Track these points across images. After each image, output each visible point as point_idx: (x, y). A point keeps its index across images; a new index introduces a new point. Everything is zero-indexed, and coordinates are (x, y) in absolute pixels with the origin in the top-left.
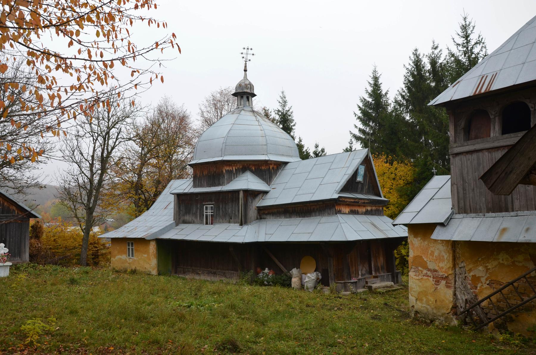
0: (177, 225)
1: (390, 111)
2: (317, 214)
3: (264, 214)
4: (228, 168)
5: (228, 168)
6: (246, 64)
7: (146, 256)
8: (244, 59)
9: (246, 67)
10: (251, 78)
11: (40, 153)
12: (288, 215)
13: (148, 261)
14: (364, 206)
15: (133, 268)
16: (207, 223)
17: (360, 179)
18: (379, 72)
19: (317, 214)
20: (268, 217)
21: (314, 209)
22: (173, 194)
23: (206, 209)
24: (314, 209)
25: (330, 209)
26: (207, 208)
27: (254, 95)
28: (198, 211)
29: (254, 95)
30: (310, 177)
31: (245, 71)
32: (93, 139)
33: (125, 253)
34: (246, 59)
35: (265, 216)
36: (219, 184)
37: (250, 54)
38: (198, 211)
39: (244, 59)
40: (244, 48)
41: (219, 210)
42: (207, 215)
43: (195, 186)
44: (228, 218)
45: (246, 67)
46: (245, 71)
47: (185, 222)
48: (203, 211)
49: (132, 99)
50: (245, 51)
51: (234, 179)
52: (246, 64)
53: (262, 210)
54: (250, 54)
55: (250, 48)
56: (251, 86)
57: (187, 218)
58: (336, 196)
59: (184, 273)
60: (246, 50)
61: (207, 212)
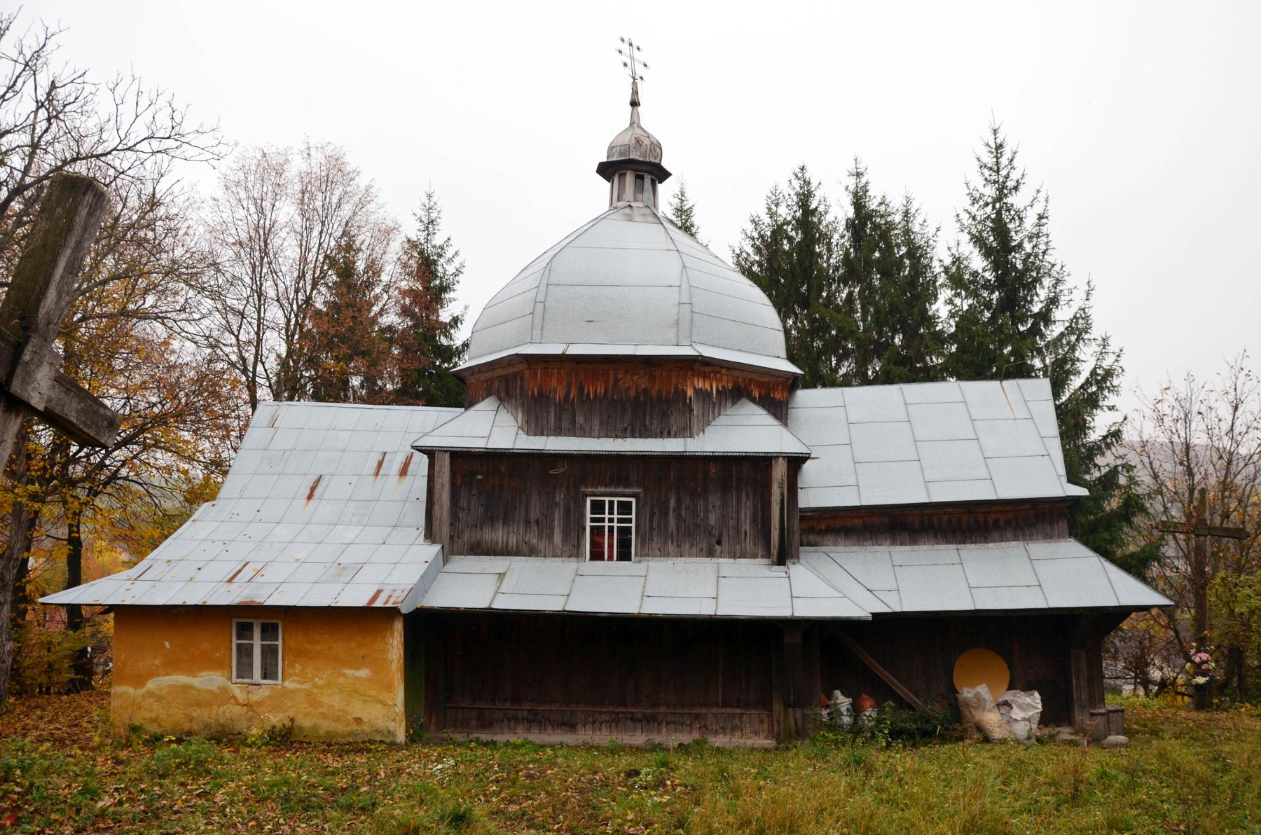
0: (446, 561)
2: (1009, 535)
3: (811, 530)
4: (700, 384)
5: (700, 384)
6: (634, 83)
7: (364, 673)
9: (635, 92)
10: (654, 123)
11: (346, 272)
12: (906, 536)
13: (370, 694)
15: (276, 719)
16: (597, 555)
18: (813, 175)
19: (1009, 535)
20: (829, 539)
21: (996, 522)
23: (598, 507)
24: (996, 522)
25: (1051, 523)
28: (558, 516)
31: (634, 104)
33: (221, 665)
35: (812, 538)
36: (665, 432)
38: (558, 516)
40: (623, 40)
41: (666, 514)
44: (712, 543)
45: (635, 92)
46: (634, 104)
47: (478, 549)
48: (583, 516)
51: (714, 418)
52: (634, 83)
53: (810, 518)
56: (657, 147)
57: (498, 535)
59: (486, 725)
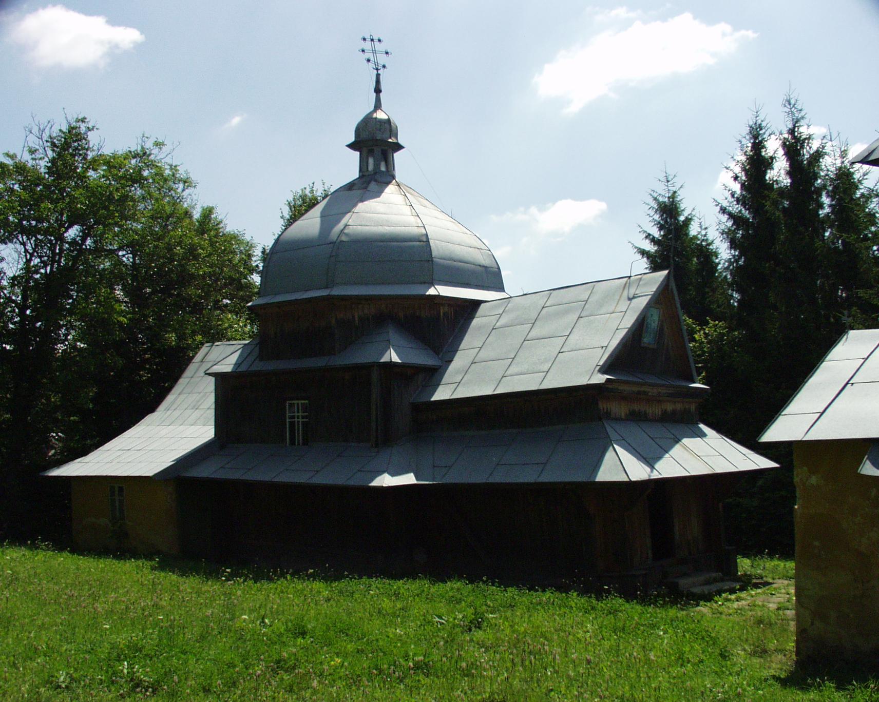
1: (858, 196)
6: (378, 76)
8: (371, 65)
9: (378, 82)
14: (659, 401)
17: (647, 340)
18: (806, 104)
22: (210, 374)
26: (291, 405)
27: (398, 147)
29: (398, 147)
30: (533, 334)
31: (378, 90)
32: (26, 251)
34: (376, 64)
37: (381, 53)
39: (371, 65)
40: (364, 39)
42: (292, 424)
43: (261, 357)
45: (378, 82)
46: (378, 90)
49: (26, 149)
50: (367, 45)
52: (378, 76)
54: (381, 53)
55: (376, 38)
58: (600, 379)
60: (368, 43)
61: (293, 417)
